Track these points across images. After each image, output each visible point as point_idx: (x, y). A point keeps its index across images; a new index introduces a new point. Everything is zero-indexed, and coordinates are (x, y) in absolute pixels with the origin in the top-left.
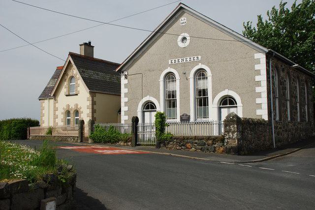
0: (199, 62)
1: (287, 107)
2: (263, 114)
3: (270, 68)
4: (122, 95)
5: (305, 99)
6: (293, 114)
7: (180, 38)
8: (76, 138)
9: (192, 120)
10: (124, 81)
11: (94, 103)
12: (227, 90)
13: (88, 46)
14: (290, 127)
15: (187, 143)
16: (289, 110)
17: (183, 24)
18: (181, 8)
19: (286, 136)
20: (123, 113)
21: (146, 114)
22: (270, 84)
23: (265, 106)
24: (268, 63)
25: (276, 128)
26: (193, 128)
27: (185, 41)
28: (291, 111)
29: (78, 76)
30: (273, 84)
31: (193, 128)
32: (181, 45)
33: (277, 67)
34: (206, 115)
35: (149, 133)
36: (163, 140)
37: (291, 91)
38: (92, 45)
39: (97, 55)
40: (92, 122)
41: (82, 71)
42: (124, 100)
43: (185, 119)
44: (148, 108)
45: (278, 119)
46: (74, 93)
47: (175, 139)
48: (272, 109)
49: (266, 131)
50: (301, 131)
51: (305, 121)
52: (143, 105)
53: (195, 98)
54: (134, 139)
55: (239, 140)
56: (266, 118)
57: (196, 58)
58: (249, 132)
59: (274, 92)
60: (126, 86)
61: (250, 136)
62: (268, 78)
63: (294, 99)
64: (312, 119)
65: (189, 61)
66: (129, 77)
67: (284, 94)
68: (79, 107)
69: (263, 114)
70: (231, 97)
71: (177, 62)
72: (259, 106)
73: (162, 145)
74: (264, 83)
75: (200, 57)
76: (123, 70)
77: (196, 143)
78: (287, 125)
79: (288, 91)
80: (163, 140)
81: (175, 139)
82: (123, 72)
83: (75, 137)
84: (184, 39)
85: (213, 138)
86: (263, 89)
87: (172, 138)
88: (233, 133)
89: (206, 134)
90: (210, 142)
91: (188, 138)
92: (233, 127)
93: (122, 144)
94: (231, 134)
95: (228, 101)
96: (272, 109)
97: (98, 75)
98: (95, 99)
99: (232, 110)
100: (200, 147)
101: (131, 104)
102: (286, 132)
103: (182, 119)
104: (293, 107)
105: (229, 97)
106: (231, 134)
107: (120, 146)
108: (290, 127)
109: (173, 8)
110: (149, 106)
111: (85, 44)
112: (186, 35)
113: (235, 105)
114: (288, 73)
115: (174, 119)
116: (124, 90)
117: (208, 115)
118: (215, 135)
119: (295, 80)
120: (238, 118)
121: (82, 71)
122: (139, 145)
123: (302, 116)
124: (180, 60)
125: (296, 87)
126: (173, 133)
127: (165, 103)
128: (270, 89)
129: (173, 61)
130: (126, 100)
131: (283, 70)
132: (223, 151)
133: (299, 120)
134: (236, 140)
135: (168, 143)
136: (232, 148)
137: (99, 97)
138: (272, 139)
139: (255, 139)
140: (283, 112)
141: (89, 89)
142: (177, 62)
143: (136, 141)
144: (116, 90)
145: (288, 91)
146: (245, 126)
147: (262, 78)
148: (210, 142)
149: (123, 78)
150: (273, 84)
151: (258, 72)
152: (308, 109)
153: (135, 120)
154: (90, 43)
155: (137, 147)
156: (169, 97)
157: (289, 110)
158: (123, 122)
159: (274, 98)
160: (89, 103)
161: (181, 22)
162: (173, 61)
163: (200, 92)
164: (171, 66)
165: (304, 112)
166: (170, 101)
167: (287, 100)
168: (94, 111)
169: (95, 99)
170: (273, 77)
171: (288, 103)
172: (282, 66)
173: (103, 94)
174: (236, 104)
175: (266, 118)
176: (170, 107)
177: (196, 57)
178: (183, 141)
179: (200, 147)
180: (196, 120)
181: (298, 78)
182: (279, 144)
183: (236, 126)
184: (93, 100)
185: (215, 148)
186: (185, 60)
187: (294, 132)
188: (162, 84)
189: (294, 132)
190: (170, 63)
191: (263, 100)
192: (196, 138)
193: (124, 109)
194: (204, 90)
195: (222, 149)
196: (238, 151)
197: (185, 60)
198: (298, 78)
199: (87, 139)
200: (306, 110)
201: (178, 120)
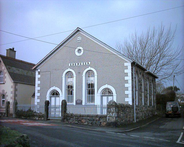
0: (89, 66)
1: (142, 97)
2: (129, 101)
3: (134, 72)
4: (36, 85)
5: (152, 91)
6: (146, 101)
7: (77, 50)
8: (4, 114)
9: (83, 104)
10: (37, 76)
11: (16, 90)
12: (107, 85)
13: (12, 51)
14: (144, 109)
15: (83, 119)
16: (143, 98)
17: (79, 41)
18: (78, 31)
19: (141, 115)
20: (36, 97)
21: (103, 97)
22: (133, 82)
23: (130, 96)
24: (132, 69)
25: (136, 110)
26: (87, 110)
27: (80, 51)
28: (144, 100)
29: (6, 71)
30: (135, 82)
31: (87, 110)
32: (77, 54)
33: (137, 72)
34: (93, 100)
35: (56, 113)
36: (66, 117)
37: (144, 87)
38: (14, 50)
39: (18, 57)
40: (16, 104)
41: (9, 68)
42: (37, 88)
43: (79, 103)
44: (53, 94)
45: (137, 104)
46: (2, 83)
47: (74, 116)
48: (134, 98)
49: (130, 112)
50: (149, 112)
51: (152, 105)
52: (50, 93)
53: (65, 90)
54: (46, 117)
55: (116, 117)
56: (131, 104)
57: (87, 63)
58: (122, 112)
59: (135, 87)
60: (39, 79)
61: (122, 115)
62: (132, 78)
63: (146, 92)
64: (155, 104)
65: (82, 65)
66: (40, 73)
67: (141, 88)
68: (5, 92)
69: (129, 101)
70: (108, 89)
71: (74, 65)
72: (127, 96)
73: (65, 120)
74: (130, 81)
75: (89, 63)
76: (37, 68)
77: (88, 119)
78: (142, 108)
79: (143, 87)
80: (66, 117)
81: (74, 116)
82: (37, 70)
83: (3, 113)
84: (80, 50)
85: (99, 116)
86: (129, 85)
87: (72, 116)
88: (113, 113)
89: (92, 113)
90: (98, 119)
91: (83, 116)
92: (113, 109)
93: (37, 118)
94: (111, 114)
95: (107, 92)
96: (134, 98)
97: (19, 70)
98: (17, 87)
99: (110, 98)
100: (91, 122)
101: (43, 92)
102: (142, 112)
103: (77, 103)
104: (146, 97)
105: (108, 89)
106: (111, 114)
107: (35, 120)
108: (144, 109)
109: (74, 29)
110: (55, 94)
111: (10, 49)
112: (81, 48)
113: (112, 95)
114: (143, 75)
115: (72, 102)
116: (37, 82)
117: (94, 101)
118: (104, 114)
119: (147, 79)
120: (116, 103)
121: (9, 68)
122: (49, 120)
123: (150, 102)
124: (77, 64)
125: (147, 84)
126: (69, 113)
127: (66, 91)
128: (133, 85)
129: (72, 65)
130: (39, 88)
131: (140, 74)
132: (106, 125)
133: (148, 104)
134: (114, 118)
135: (69, 119)
136: (111, 123)
137: (20, 86)
138: (134, 117)
139: (124, 117)
140: (140, 99)
141: (13, 80)
142: (74, 65)
143: (47, 117)
144: (31, 82)
145: (143, 87)
146: (120, 108)
147: (129, 78)
148: (98, 119)
149: (37, 73)
150: (135, 82)
151: (127, 75)
152: (153, 98)
153: (47, 103)
154: (13, 49)
155: (48, 121)
156: (89, 87)
157: (143, 98)
158: (36, 104)
159: (136, 90)
160: (12, 90)
161: (78, 39)
162: (72, 65)
163: (89, 84)
164: (71, 67)
165: (151, 100)
166: (69, 91)
167: (142, 92)
168: (15, 95)
169: (17, 87)
170: (135, 77)
171: (143, 94)
172: (140, 71)
173: (22, 84)
174: (113, 94)
175: (131, 104)
176: (69, 94)
177: (84, 63)
178: (79, 118)
179: (91, 122)
180: (86, 104)
181: (148, 78)
182: (138, 120)
183: (114, 109)
184: (15, 88)
185: (101, 123)
186: (80, 64)
187: (145, 112)
188: (64, 79)
189: (145, 112)
190: (70, 66)
191: (129, 92)
192: (88, 116)
193: (37, 94)
194: (92, 84)
195: (105, 123)
196: (115, 125)
197: (80, 64)
198: (148, 78)
199: (12, 115)
200: (152, 99)
201: (74, 103)
